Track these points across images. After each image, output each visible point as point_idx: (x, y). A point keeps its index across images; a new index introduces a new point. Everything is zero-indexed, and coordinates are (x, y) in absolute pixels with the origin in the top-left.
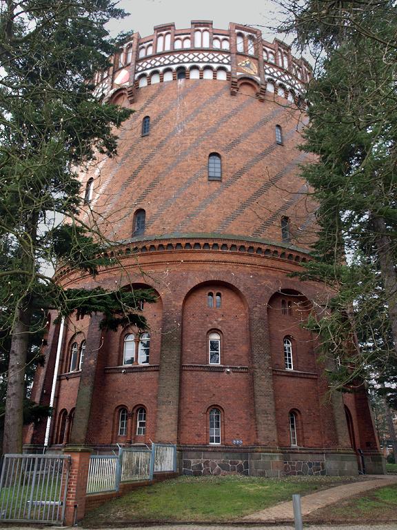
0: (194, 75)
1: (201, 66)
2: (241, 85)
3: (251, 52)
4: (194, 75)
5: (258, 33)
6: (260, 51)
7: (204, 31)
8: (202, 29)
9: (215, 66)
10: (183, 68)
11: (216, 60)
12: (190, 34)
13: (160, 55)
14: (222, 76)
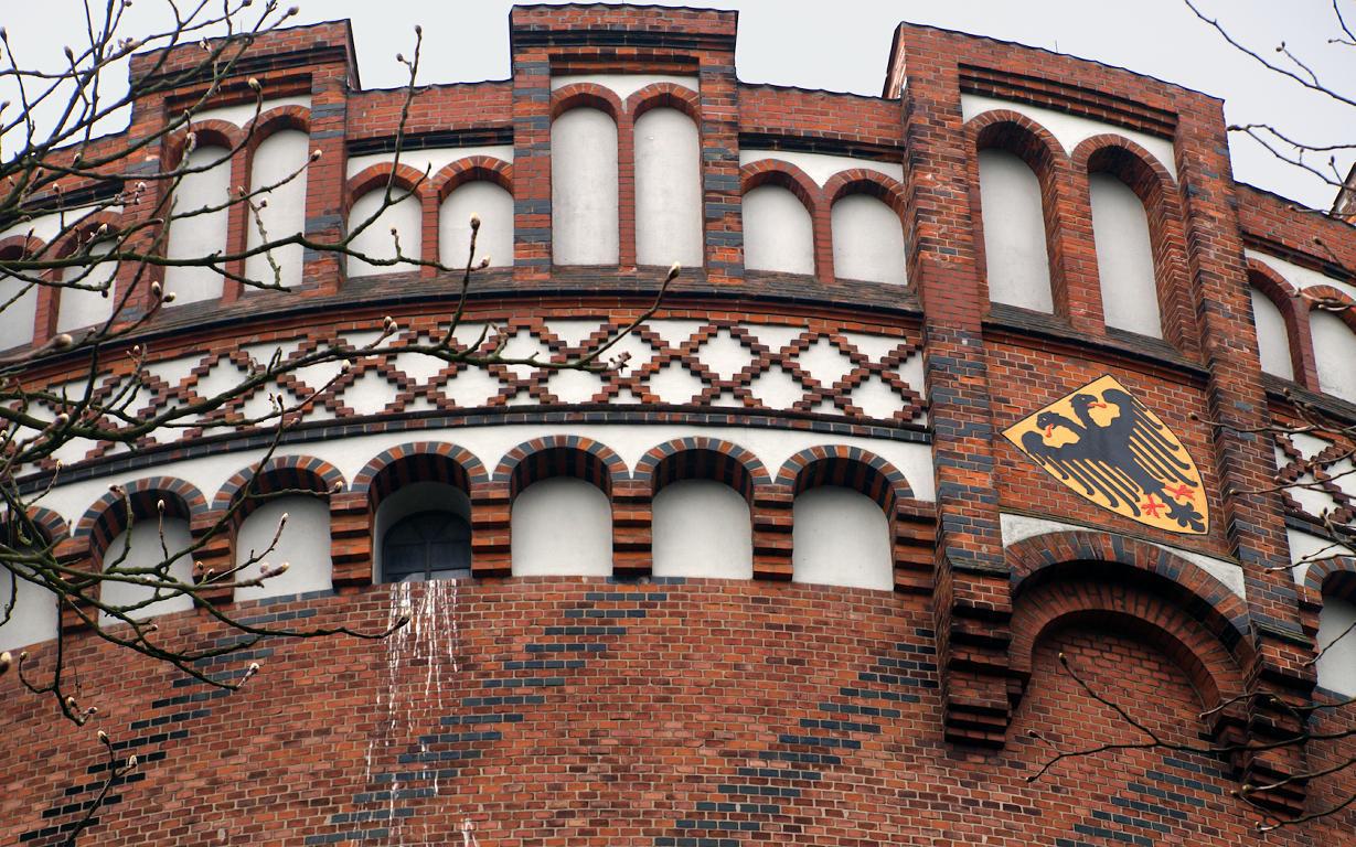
0: (561, 543)
1: (631, 447)
2: (1055, 636)
3: (1130, 299)
4: (561, 543)
5: (1187, 124)
6: (1224, 298)
7: (647, 105)
8: (624, 88)
9: (773, 452)
10: (450, 470)
11: (776, 392)
12: (503, 136)
13: (200, 334)
14: (845, 554)
